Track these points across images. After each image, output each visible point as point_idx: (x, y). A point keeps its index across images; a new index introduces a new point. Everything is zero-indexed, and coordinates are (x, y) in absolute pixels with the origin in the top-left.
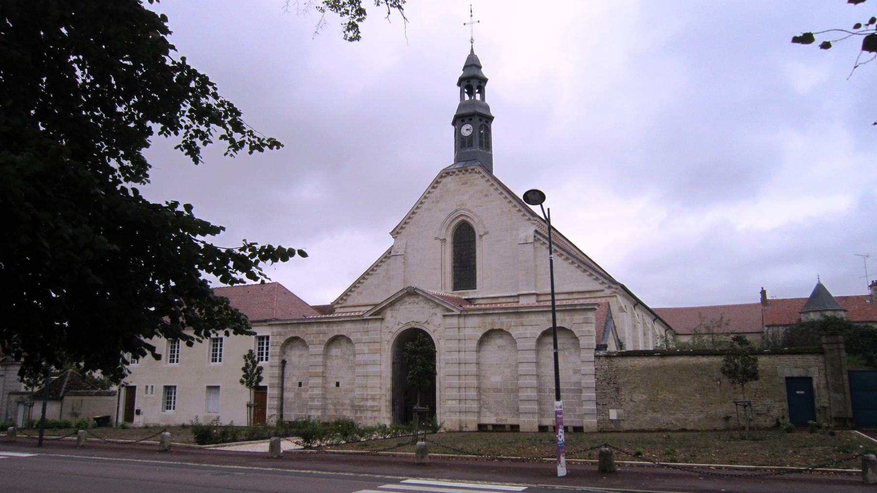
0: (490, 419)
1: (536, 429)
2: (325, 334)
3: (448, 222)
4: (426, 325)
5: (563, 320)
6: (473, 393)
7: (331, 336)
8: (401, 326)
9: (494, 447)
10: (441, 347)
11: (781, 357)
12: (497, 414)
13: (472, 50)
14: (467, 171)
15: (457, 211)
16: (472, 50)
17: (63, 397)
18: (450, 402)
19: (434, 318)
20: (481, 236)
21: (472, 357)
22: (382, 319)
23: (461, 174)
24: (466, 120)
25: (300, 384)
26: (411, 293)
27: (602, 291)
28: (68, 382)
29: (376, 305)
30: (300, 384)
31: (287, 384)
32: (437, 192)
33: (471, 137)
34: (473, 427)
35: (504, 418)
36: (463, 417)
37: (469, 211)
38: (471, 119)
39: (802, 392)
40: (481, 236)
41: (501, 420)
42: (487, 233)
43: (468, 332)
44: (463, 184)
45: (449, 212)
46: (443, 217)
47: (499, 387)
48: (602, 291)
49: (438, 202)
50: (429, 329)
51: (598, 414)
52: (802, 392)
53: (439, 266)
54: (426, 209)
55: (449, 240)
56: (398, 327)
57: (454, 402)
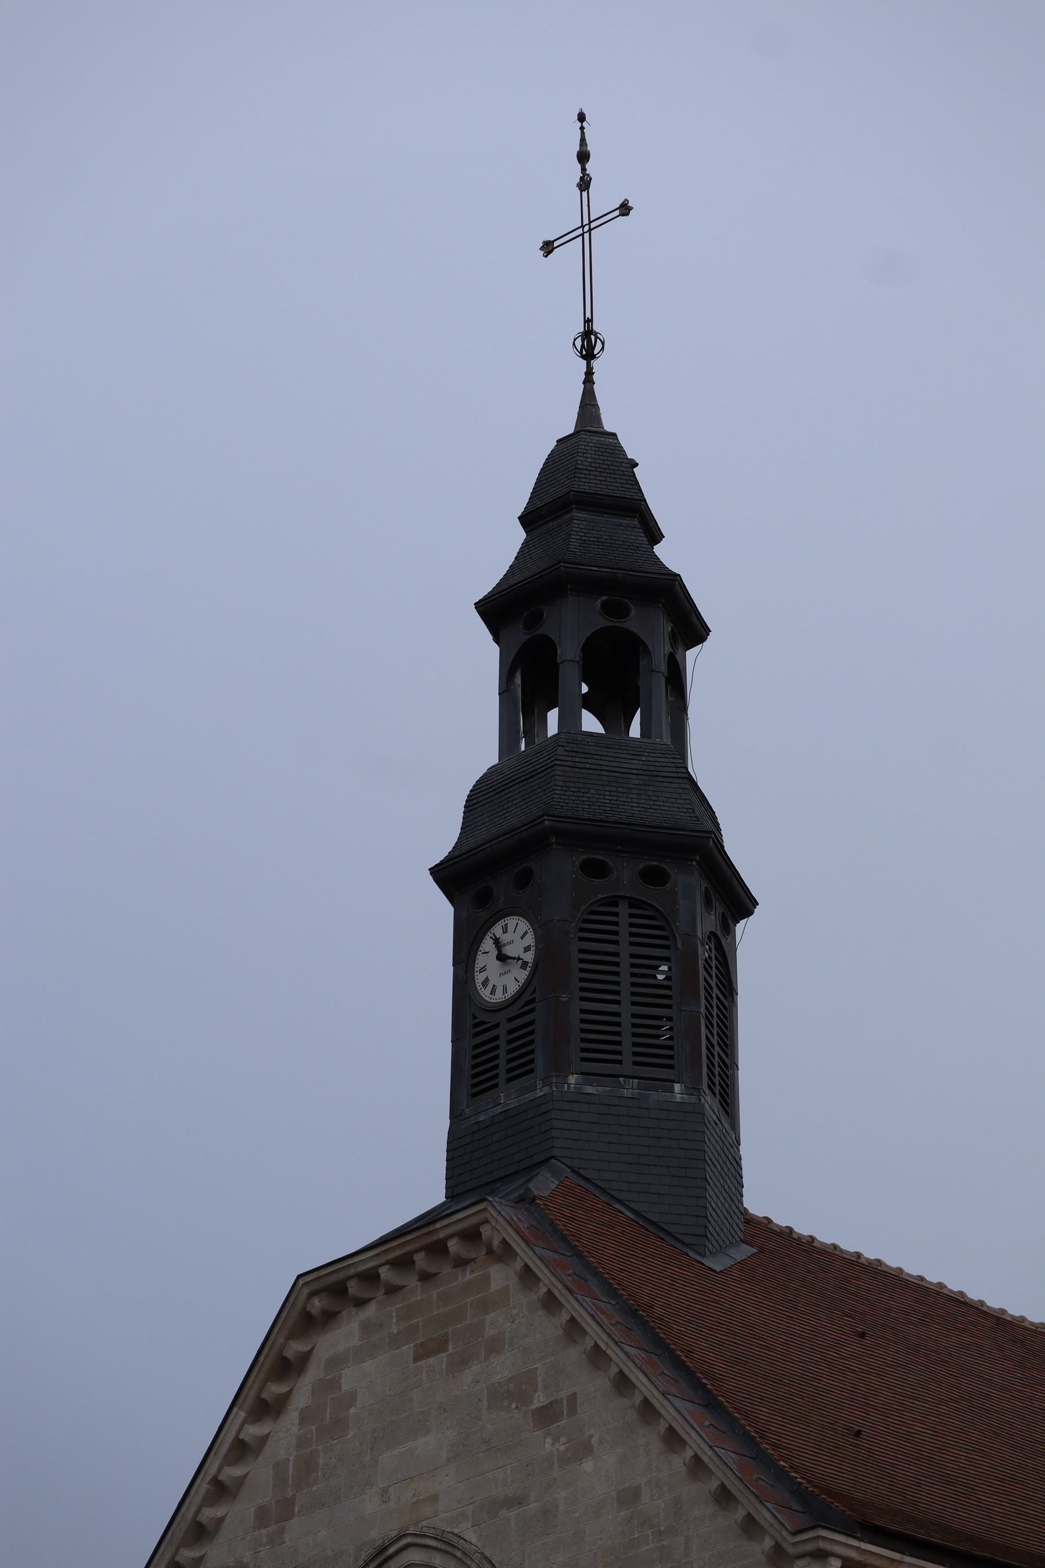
13: (589, 405)
16: (589, 405)
32: (284, 1434)
44: (424, 1352)
49: (286, 1509)
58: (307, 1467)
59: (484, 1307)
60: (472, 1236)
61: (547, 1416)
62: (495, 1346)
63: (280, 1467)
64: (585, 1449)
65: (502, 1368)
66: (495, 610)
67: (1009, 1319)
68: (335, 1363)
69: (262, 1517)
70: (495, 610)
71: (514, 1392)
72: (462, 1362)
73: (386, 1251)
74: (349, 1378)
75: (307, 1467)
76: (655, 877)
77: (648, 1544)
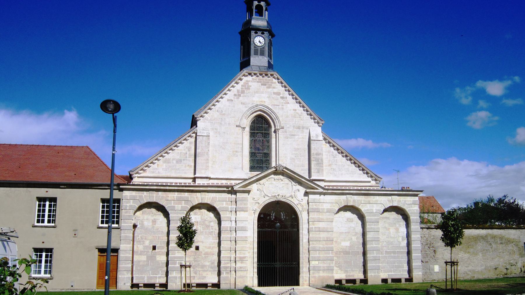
1: (380, 283)
2: (187, 201)
3: (249, 114)
4: (290, 199)
5: (313, 206)
7: (195, 203)
8: (267, 198)
10: (303, 217)
11: (521, 230)
12: (346, 271)
14: (266, 75)
15: (257, 106)
19: (297, 193)
22: (248, 192)
23: (261, 77)
24: (259, 33)
25: (154, 248)
27: (370, 182)
29: (245, 180)
30: (154, 248)
31: (138, 247)
35: (351, 274)
37: (268, 108)
38: (263, 33)
41: (349, 276)
42: (283, 128)
44: (262, 85)
45: (250, 106)
47: (348, 250)
48: (370, 182)
49: (240, 95)
51: (423, 269)
53: (240, 150)
54: (228, 100)
55: (248, 129)
56: (264, 199)
59: (272, 83)
61: (282, 98)
62: (274, 88)
64: (288, 103)
65: (275, 90)
72: (269, 88)
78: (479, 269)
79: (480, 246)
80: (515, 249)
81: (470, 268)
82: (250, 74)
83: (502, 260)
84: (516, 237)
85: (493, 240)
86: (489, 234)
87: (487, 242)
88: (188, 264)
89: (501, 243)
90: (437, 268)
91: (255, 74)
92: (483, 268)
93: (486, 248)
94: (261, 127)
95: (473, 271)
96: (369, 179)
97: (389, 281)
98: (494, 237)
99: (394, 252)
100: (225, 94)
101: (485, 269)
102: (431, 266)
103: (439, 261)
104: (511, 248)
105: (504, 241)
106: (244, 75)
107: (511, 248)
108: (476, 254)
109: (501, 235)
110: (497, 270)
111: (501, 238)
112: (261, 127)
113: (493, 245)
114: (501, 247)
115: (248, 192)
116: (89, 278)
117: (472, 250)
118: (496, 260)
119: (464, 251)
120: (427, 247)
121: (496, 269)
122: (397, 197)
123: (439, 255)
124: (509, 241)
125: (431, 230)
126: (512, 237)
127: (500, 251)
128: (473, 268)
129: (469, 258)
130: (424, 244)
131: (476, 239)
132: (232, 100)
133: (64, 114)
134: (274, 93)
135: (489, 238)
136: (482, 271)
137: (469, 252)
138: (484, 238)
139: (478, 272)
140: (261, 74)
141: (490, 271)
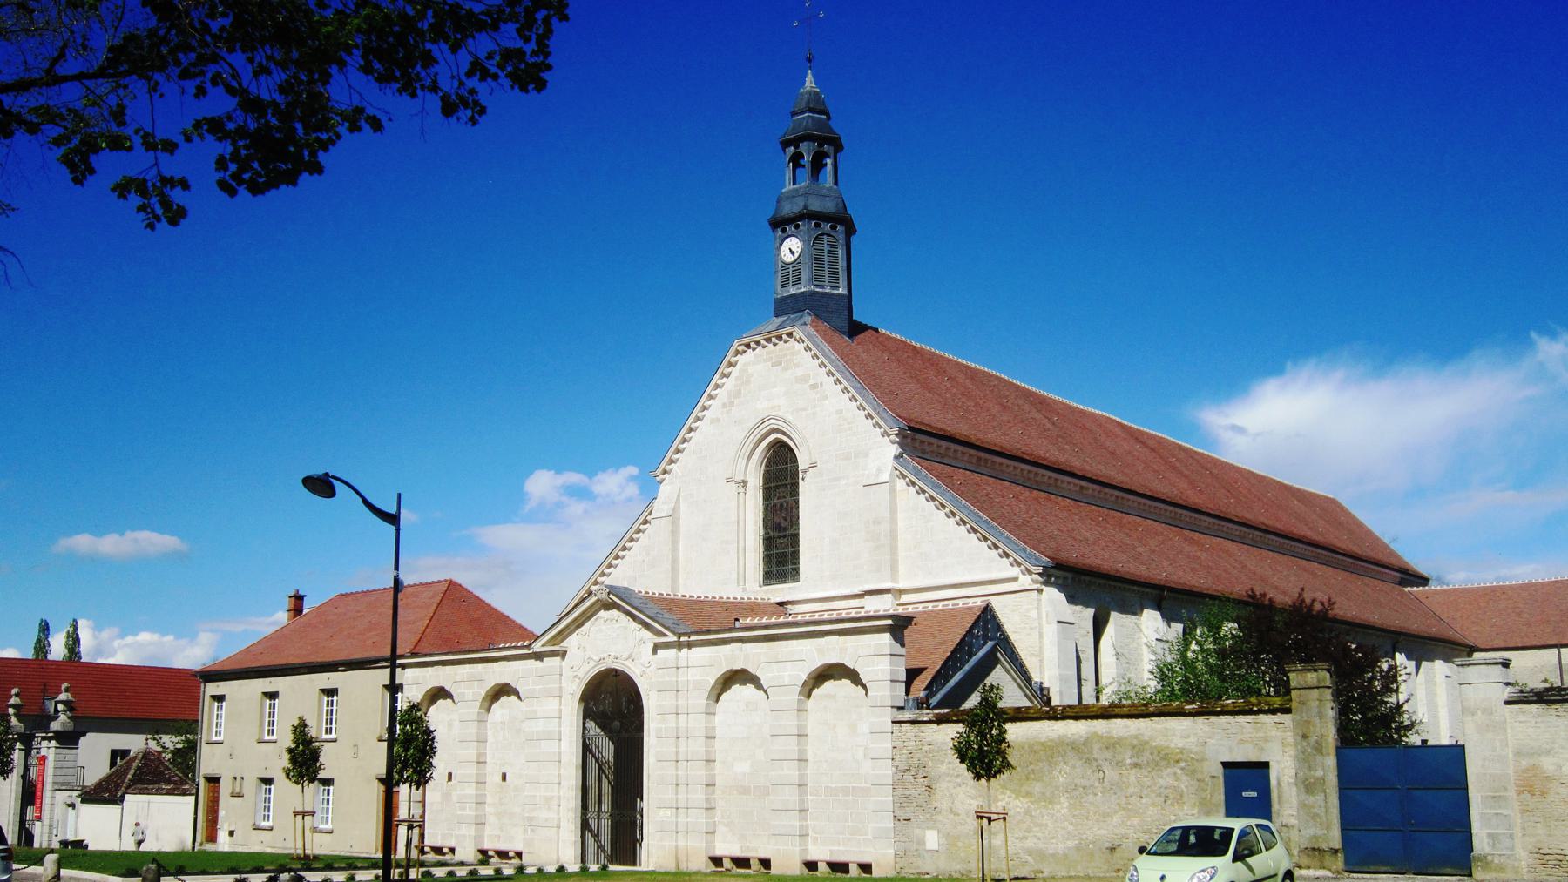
0: (728, 847)
6: (699, 795)
8: (592, 664)
9: (238, 864)
10: (652, 705)
11: (1213, 718)
14: (779, 338)
17: (123, 796)
18: (662, 812)
20: (805, 472)
21: (697, 723)
22: (563, 654)
23: (781, 343)
26: (618, 601)
27: (1015, 579)
28: (138, 768)
33: (797, 262)
34: (700, 863)
36: (682, 843)
39: (1254, 794)
40: (805, 472)
42: (813, 466)
43: (694, 675)
45: (751, 424)
46: (741, 436)
48: (1015, 579)
49: (732, 404)
50: (635, 672)
52: (1254, 794)
56: (587, 667)
57: (668, 812)
58: (738, 394)
60: (790, 335)
61: (814, 387)
62: (797, 366)
63: (729, 393)
64: (826, 397)
65: (800, 372)
66: (295, 184)
67: (1320, 665)
68: (746, 364)
69: (724, 405)
70: (295, 184)
71: (805, 379)
72: (786, 369)
73: (766, 627)
74: (751, 369)
75: (738, 394)
76: (833, 228)
77: (797, 282)
78: (1060, 846)
79: (1064, 773)
80: (1184, 783)
81: (1030, 843)
82: (748, 346)
83: (1136, 821)
84: (1190, 743)
85: (1108, 755)
86: (1096, 733)
87: (1088, 761)
88: (308, 808)
89: (1136, 765)
90: (932, 840)
91: (758, 343)
92: (1071, 844)
93: (1085, 782)
94: (781, 472)
95: (1041, 855)
96: (1015, 571)
97: (822, 867)
98: (1112, 744)
99: (846, 791)
100: (705, 408)
101: (1078, 848)
102: (918, 831)
103: (940, 818)
104: (1170, 781)
105: (1143, 759)
106: (738, 353)
107: (1170, 781)
108: (1051, 800)
109: (1136, 737)
110: (1117, 855)
111: (1139, 747)
112: (781, 472)
113: (1111, 773)
114: (1132, 778)
115: (563, 654)
116: (551, 830)
117: (1037, 787)
118: (1116, 819)
119: (1013, 791)
120: (908, 777)
121: (1112, 849)
122: (836, 638)
123: (941, 800)
124: (1165, 758)
125: (923, 727)
126: (1177, 743)
127: (1131, 790)
128: (1041, 845)
129: (1027, 812)
130: (903, 766)
131: (1053, 751)
132: (718, 420)
133: (1530, 344)
134: (798, 380)
135: (1096, 747)
136: (1065, 855)
137: (1028, 794)
138: (1077, 747)
139: (1053, 855)
140: (769, 340)
141: (1092, 855)
